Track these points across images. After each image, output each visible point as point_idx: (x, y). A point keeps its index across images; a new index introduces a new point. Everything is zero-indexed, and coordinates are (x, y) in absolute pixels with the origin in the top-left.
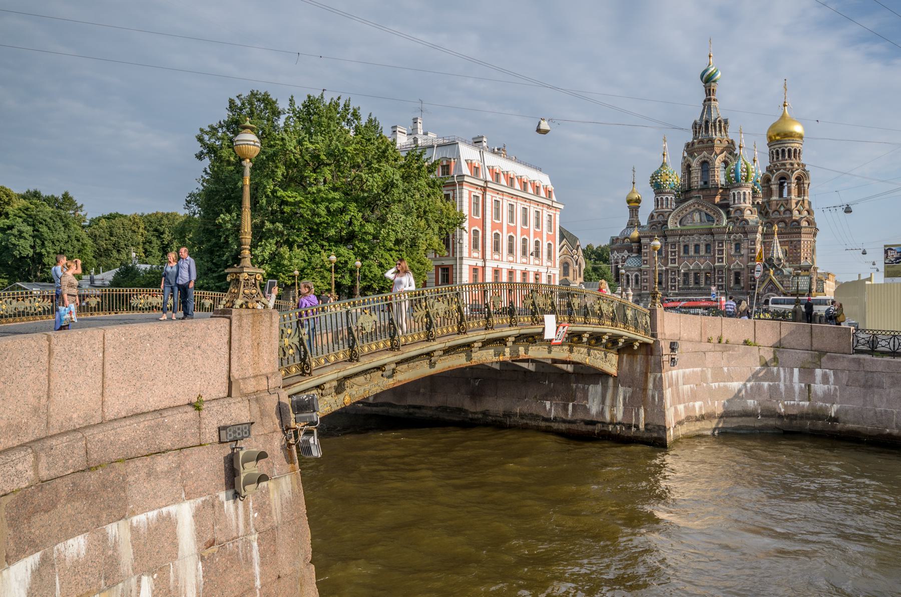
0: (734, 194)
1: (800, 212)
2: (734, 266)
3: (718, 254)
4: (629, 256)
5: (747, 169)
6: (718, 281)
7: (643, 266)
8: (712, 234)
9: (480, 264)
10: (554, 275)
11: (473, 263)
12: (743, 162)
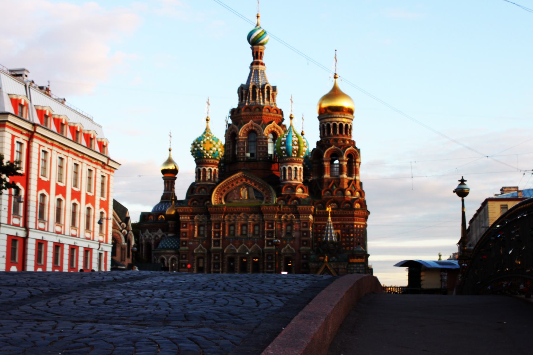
1: (352, 194)
2: (285, 250)
3: (268, 237)
4: (163, 236)
5: (299, 142)
6: (268, 268)
7: (182, 248)
9: (21, 233)
10: (106, 252)
11: (13, 232)
12: (294, 134)
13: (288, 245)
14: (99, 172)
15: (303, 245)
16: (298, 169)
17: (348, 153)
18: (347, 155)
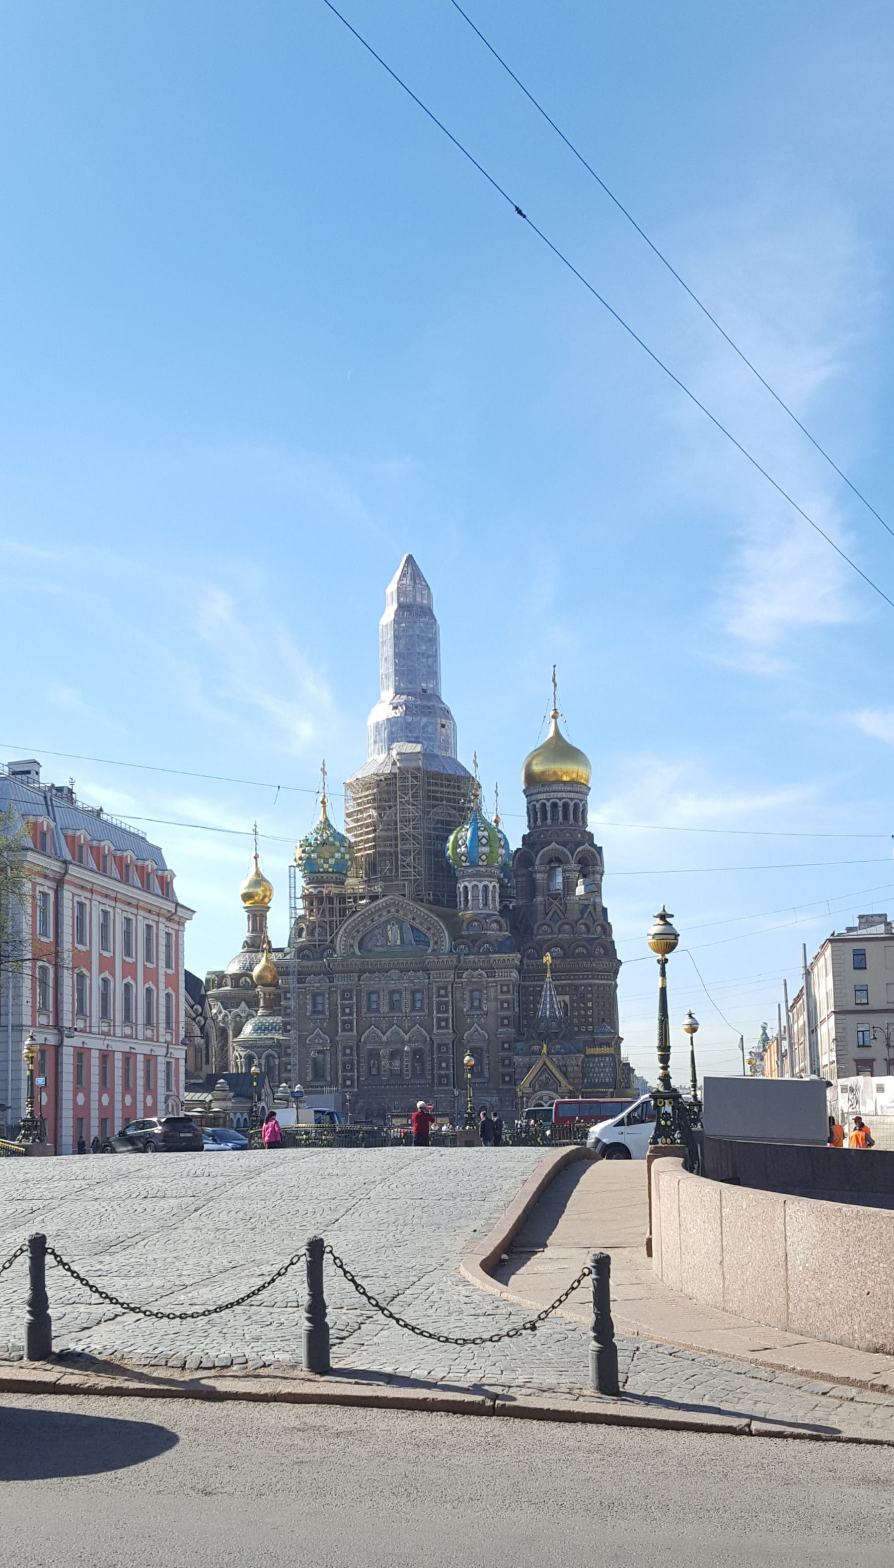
0: (466, 888)
3: (439, 1012)
8: (426, 970)
10: (177, 1059)
13: (475, 1025)
14: (163, 927)
15: (503, 1025)
16: (491, 888)
17: (579, 856)
18: (578, 859)
